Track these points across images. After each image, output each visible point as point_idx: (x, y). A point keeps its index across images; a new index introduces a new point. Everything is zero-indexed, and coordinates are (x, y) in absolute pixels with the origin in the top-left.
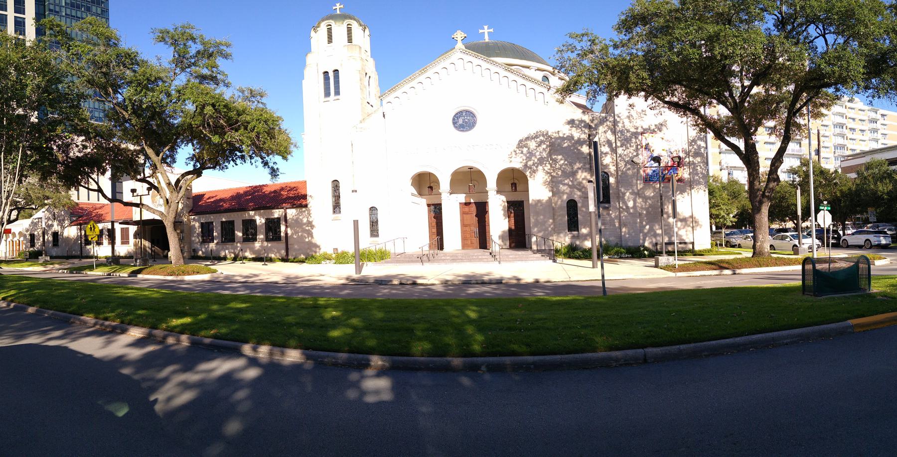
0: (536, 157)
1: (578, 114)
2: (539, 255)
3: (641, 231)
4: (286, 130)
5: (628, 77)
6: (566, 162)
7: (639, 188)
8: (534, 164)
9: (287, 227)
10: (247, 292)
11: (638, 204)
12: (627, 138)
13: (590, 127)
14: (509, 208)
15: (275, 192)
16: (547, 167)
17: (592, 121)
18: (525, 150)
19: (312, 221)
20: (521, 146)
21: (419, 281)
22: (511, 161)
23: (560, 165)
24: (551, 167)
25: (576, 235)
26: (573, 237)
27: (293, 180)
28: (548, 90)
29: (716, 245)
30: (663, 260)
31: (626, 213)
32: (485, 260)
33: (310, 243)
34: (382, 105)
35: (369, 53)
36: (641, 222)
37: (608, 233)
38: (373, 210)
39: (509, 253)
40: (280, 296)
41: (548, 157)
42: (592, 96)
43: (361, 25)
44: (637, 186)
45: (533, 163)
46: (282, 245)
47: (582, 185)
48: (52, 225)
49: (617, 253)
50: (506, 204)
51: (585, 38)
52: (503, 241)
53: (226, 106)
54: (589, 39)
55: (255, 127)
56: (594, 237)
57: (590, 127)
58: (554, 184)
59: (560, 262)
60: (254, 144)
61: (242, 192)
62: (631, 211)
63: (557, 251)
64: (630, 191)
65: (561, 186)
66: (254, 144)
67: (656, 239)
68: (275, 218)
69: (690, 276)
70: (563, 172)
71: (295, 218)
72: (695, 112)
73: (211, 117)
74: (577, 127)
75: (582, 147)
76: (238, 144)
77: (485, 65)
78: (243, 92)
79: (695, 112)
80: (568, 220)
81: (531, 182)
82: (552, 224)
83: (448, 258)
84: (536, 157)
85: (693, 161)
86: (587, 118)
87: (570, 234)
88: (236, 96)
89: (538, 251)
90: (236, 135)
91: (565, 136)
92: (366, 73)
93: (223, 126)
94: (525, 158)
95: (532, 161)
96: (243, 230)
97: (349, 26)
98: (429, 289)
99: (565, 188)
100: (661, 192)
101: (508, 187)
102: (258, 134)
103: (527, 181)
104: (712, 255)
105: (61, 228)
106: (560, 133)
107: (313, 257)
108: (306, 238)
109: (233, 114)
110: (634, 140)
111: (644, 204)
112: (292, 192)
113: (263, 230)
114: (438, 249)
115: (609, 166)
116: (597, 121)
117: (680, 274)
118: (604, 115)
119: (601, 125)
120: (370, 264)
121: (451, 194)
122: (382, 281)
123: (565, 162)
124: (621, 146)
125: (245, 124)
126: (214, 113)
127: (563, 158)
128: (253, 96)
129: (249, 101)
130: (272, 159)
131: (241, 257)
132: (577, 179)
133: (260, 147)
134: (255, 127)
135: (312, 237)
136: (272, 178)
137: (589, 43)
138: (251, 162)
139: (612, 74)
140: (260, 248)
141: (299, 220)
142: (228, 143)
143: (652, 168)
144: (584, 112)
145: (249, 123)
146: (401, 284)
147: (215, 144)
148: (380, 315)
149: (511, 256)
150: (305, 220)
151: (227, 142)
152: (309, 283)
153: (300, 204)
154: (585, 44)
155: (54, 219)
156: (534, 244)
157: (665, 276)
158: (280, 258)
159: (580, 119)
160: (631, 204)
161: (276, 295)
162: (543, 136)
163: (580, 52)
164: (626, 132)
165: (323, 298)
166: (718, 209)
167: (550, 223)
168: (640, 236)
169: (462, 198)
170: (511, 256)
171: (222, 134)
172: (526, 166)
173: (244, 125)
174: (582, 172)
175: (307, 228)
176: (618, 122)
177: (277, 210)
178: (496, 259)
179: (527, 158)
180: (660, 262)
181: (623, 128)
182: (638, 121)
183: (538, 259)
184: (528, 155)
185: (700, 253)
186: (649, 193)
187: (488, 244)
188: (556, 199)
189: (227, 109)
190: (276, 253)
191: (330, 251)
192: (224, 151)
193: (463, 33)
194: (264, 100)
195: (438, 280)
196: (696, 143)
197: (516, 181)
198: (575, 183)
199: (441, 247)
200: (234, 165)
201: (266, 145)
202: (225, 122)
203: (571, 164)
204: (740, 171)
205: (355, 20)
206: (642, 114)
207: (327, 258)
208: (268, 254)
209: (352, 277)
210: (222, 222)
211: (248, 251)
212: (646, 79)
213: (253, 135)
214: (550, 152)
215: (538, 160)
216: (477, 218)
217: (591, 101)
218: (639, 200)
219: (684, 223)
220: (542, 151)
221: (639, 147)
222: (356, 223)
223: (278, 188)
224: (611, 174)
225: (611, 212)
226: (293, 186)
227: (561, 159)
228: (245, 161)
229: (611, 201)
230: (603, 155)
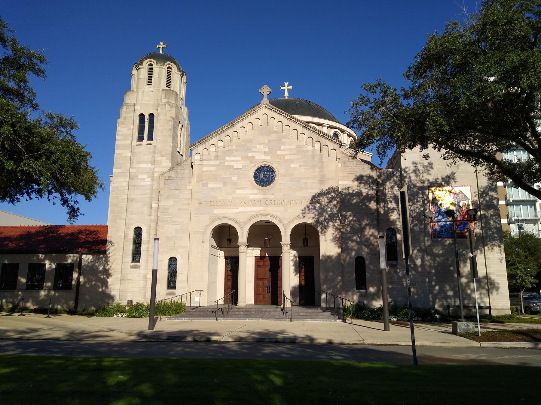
0: (327, 213)
1: (366, 171)
2: (328, 314)
4: (93, 168)
5: (424, 124)
6: (355, 219)
7: (426, 245)
8: (325, 220)
9: (80, 275)
10: (18, 351)
11: (426, 262)
13: (378, 184)
14: (300, 262)
15: (72, 234)
16: (337, 222)
17: (379, 176)
18: (318, 205)
19: (109, 269)
20: (314, 202)
21: (214, 338)
22: (304, 217)
23: (349, 221)
24: (341, 223)
25: (363, 294)
26: (361, 296)
27: (94, 224)
28: (340, 147)
29: (517, 311)
30: (462, 325)
31: (414, 272)
32: (277, 317)
33: (103, 292)
34: (191, 155)
35: (184, 101)
37: (395, 292)
38: (173, 261)
39: (300, 310)
40: (58, 355)
41: (338, 214)
42: (381, 151)
43: (179, 70)
44: (425, 243)
45: (324, 219)
46: (72, 294)
47: (369, 242)
49: (406, 315)
50: (298, 259)
51: (378, 89)
52: (293, 298)
53: (28, 129)
54: (382, 90)
55: (59, 159)
56: (386, 297)
57: (378, 184)
58: (343, 240)
59: (350, 322)
60: (55, 177)
61: (33, 231)
62: (420, 269)
63: (345, 310)
64: (418, 248)
65: (350, 242)
66: (55, 177)
67: (447, 302)
69: (498, 348)
70: (351, 228)
71: (90, 265)
72: (490, 159)
73: (7, 138)
74: (366, 183)
75: (370, 204)
76: (36, 175)
77: (285, 121)
78: (52, 118)
79: (490, 159)
80: (356, 277)
81: (321, 238)
82: (340, 281)
83: (242, 313)
84: (327, 213)
85: (484, 214)
86: (374, 174)
87: (358, 292)
88: (44, 121)
89: (327, 309)
90: (36, 165)
91: (354, 192)
92: (179, 122)
93: (20, 151)
94: (316, 213)
95: (323, 217)
96: (28, 276)
97: (169, 69)
98: (224, 348)
99: (354, 244)
100: (457, 249)
101: (300, 243)
102: (61, 167)
103: (319, 236)
104: (513, 322)
106: (349, 189)
107: (104, 309)
108: (99, 288)
109: (35, 140)
112: (91, 236)
113: (52, 277)
114: (233, 304)
115: (396, 222)
116: (384, 177)
117: (485, 344)
118: (390, 170)
119: (388, 181)
120: (164, 318)
121: (248, 247)
122: (175, 337)
123: (354, 218)
125: (48, 154)
126: (11, 135)
127: (352, 215)
128: (63, 126)
129: (57, 130)
130: (74, 197)
131: (21, 308)
132: (365, 235)
133: (61, 182)
134: (59, 159)
135: (107, 287)
136: (70, 218)
137: (381, 95)
138: (48, 198)
139: (405, 125)
140: (46, 298)
141: (95, 267)
142: (24, 172)
143: (440, 223)
144: (372, 169)
145: (52, 153)
146: (195, 341)
147: (8, 171)
148: (172, 378)
149: (301, 314)
150: (101, 268)
151: (22, 171)
152: (95, 340)
153: (98, 250)
154: (378, 96)
156: (324, 302)
157: (469, 345)
158: (68, 310)
159: (368, 175)
160: (419, 262)
161: (53, 355)
162: (334, 192)
163: (373, 105)
164: (412, 186)
165: (109, 357)
166: (514, 269)
167: (339, 280)
168: (429, 298)
169: (257, 251)
170: (301, 314)
171: (18, 160)
172: (317, 221)
173: (46, 155)
174: (370, 228)
175: (102, 277)
176: (405, 177)
177: (72, 255)
178: (287, 316)
179: (319, 213)
180: (458, 328)
181: (410, 183)
182: (425, 175)
183: (327, 318)
184: (320, 211)
185: (498, 320)
186: (437, 250)
187: (279, 300)
188: (345, 255)
189: (29, 133)
190: (63, 304)
191: (124, 303)
192: (18, 181)
193: (269, 88)
194: (74, 132)
195: (232, 337)
196: (487, 194)
197: (308, 237)
198: (363, 240)
199: (236, 303)
200: (28, 199)
201: (69, 181)
202: (24, 147)
203: (359, 220)
204: (532, 225)
205: (175, 63)
206: (428, 168)
207: (120, 310)
208: (53, 306)
209: (143, 332)
210: (4, 265)
211: (31, 301)
212: (443, 126)
213: (56, 167)
214: (340, 208)
215: (329, 216)
216: (270, 273)
217: (381, 156)
218: (427, 258)
220: (333, 207)
221: (426, 202)
222: (155, 272)
223: (76, 230)
224: (399, 230)
225: (398, 271)
226: (93, 229)
227: (350, 216)
228: (41, 196)
229: (398, 259)
230: (390, 211)
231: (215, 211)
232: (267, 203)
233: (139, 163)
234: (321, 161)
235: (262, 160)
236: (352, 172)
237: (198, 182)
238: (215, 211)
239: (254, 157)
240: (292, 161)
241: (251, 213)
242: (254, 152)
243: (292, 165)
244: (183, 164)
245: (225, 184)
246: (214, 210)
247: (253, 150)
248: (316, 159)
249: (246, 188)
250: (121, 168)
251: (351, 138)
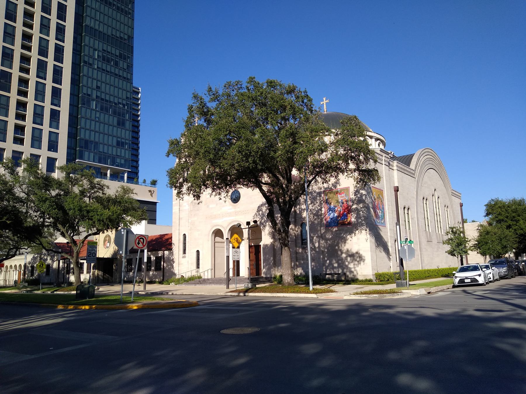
3: (324, 264)
7: (322, 233)
8: (264, 221)
9: (164, 262)
12: (315, 197)
36: (324, 258)
48: (47, 259)
64: (316, 235)
68: (159, 257)
81: (263, 233)
95: (264, 220)
105: (52, 261)
110: (318, 198)
111: (326, 244)
124: (311, 204)
155: (48, 255)
168: (323, 268)
218: (322, 242)
219: (352, 258)
230: (303, 211)
245: (217, 204)
251: (379, 141)
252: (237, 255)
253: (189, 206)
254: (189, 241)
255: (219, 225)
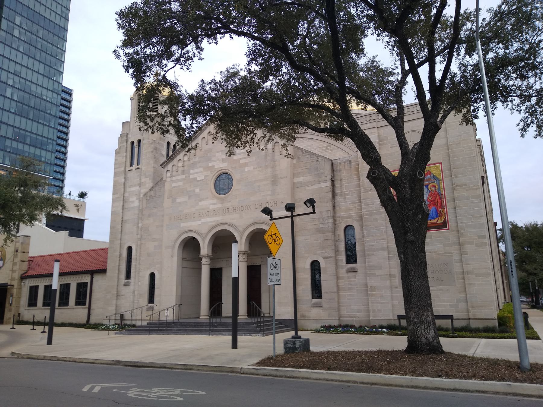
231: (183, 225)
232: (225, 211)
233: (130, 187)
234: (273, 160)
235: (221, 168)
236: (307, 167)
237: (169, 198)
238: (183, 225)
239: (214, 166)
240: (246, 165)
241: (210, 224)
242: (214, 161)
243: (247, 169)
244: (160, 182)
245: (190, 197)
246: (182, 224)
247: (213, 159)
248: (268, 159)
249: (207, 198)
250: (117, 194)
252: (277, 272)
253: (140, 201)
254: (136, 258)
255: (192, 231)
